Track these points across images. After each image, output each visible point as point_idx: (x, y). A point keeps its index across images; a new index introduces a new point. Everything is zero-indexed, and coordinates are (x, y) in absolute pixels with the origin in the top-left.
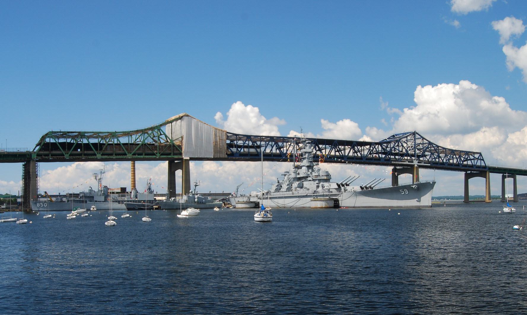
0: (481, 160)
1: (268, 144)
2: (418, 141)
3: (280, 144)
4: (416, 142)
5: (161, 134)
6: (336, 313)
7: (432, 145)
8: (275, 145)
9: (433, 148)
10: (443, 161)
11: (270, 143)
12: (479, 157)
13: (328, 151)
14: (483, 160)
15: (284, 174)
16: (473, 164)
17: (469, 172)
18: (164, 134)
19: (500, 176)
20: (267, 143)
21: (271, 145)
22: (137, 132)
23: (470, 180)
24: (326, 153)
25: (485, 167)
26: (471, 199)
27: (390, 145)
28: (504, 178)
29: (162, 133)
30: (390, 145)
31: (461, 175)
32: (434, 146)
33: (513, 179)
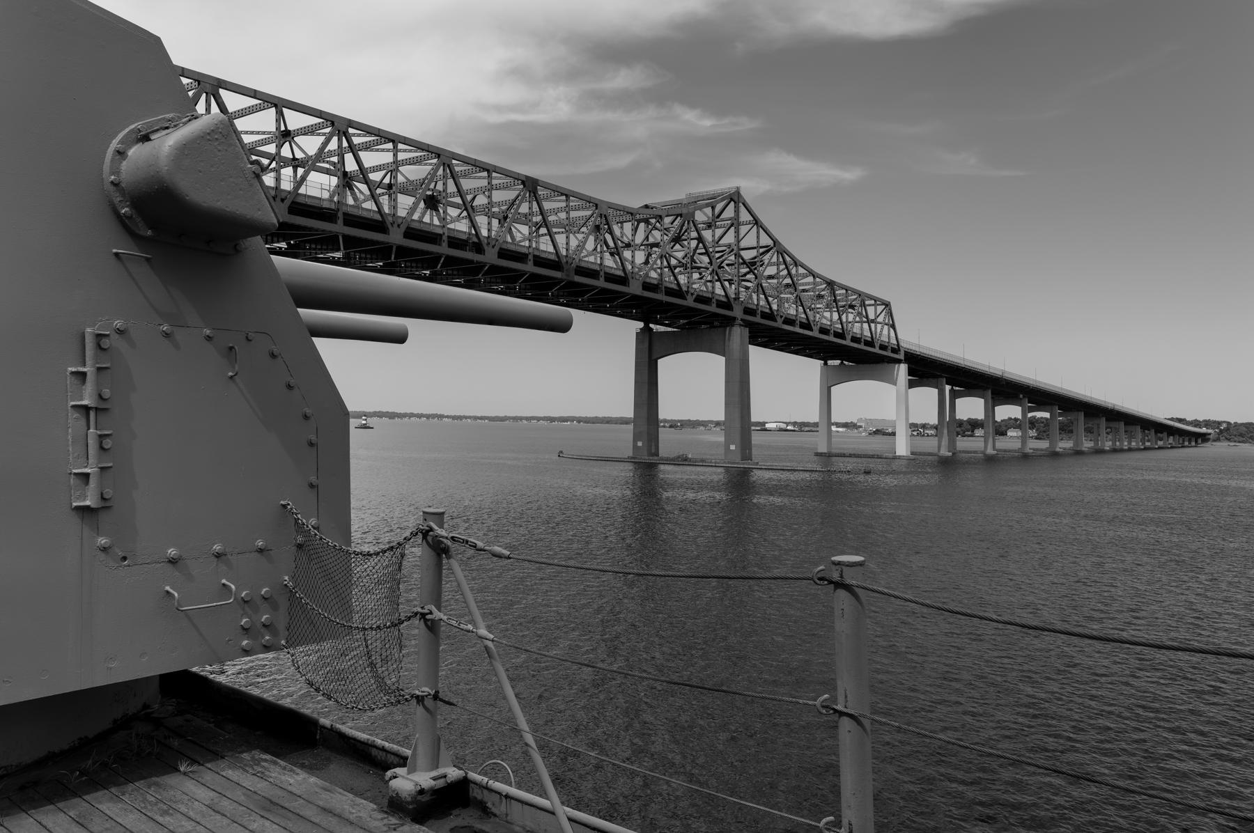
14: (893, 326)
23: (958, 401)
32: (788, 259)
33: (983, 400)
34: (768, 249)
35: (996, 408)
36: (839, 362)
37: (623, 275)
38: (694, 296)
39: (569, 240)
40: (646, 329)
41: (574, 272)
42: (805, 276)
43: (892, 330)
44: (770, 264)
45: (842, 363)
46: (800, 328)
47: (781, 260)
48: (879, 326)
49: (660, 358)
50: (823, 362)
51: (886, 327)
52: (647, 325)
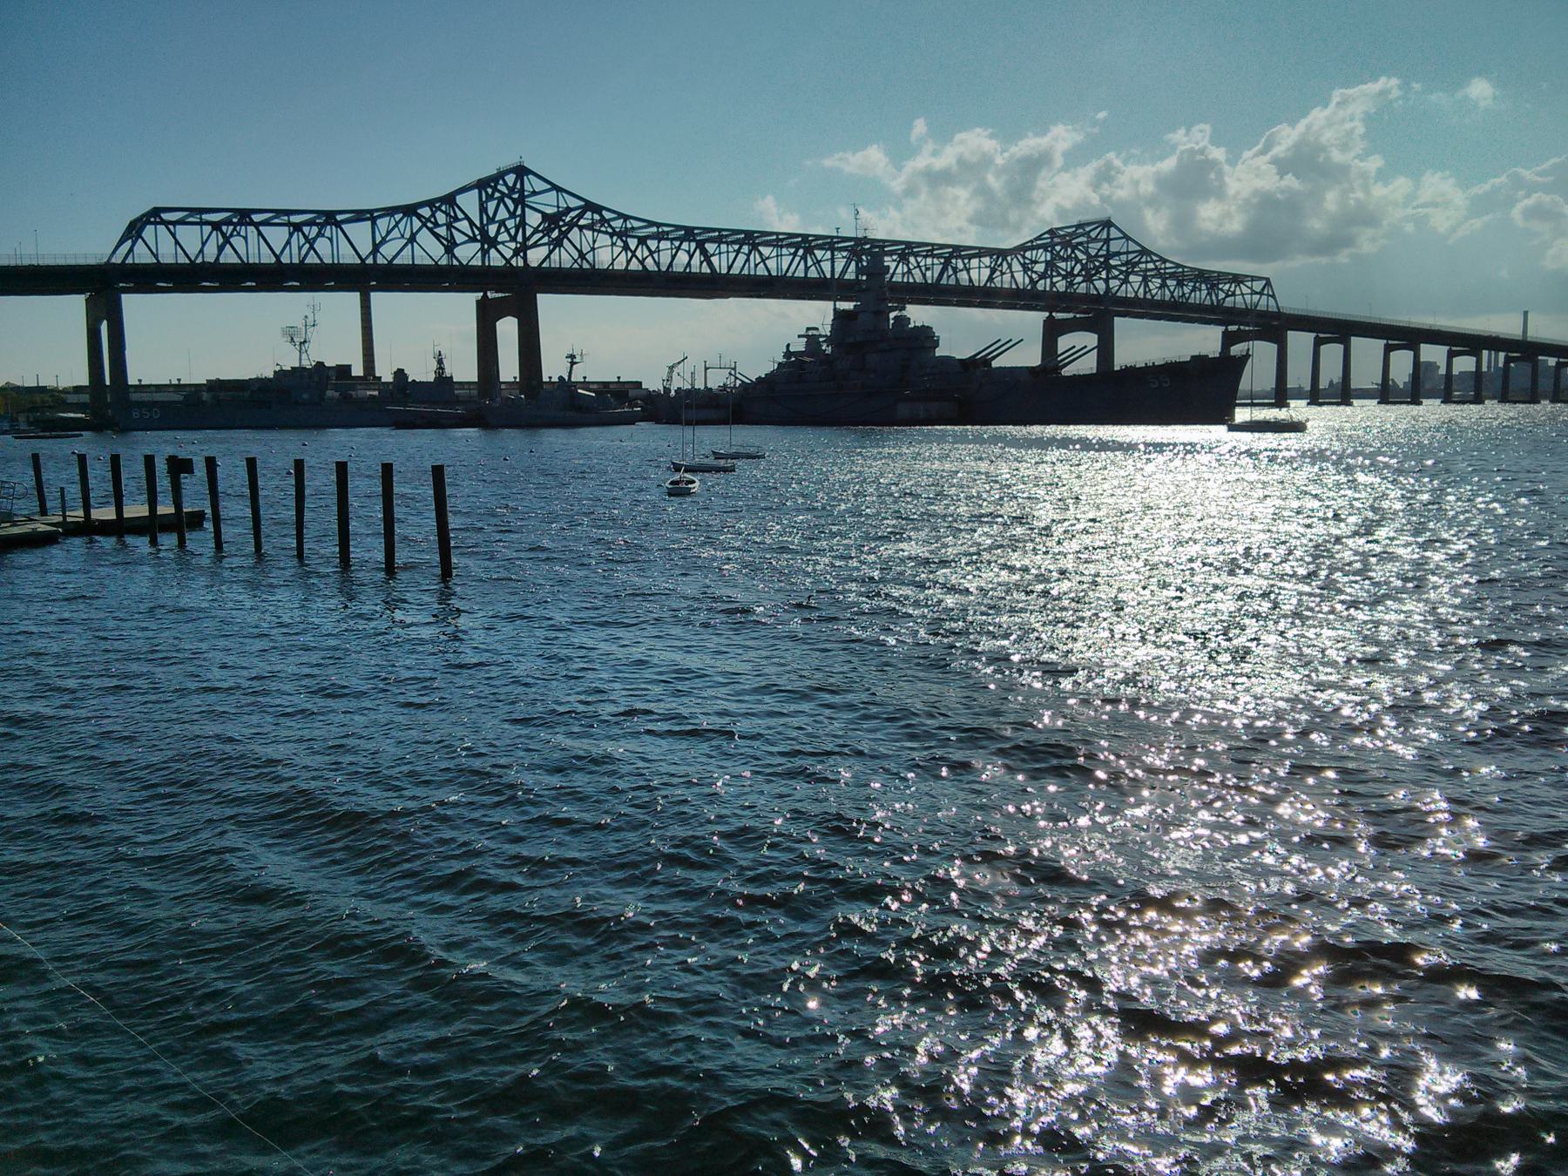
1: (678, 249)
2: (1115, 246)
3: (711, 247)
5: (457, 219)
6: (1555, 1097)
8: (698, 252)
9: (1151, 266)
10: (1172, 296)
11: (685, 245)
12: (1263, 289)
13: (786, 261)
14: (1273, 296)
15: (803, 333)
16: (828, 276)
18: (467, 218)
19: (1380, 344)
20: (677, 243)
21: (688, 252)
22: (390, 211)
28: (1388, 349)
29: (460, 215)
31: (464, 305)
32: (1155, 258)
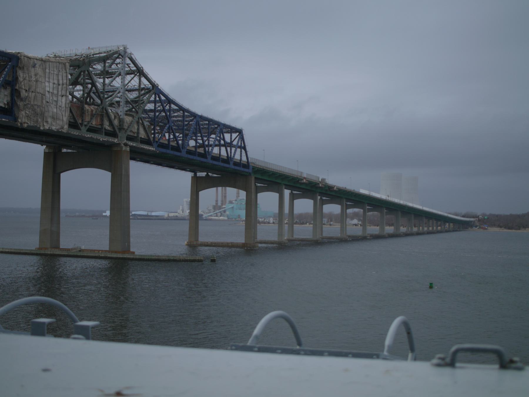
0: (240, 147)
4: (113, 83)
7: (159, 97)
14: (244, 148)
17: (204, 174)
23: (296, 202)
24: (134, 77)
25: (247, 165)
26: (339, 227)
27: (132, 79)
30: (132, 79)
32: (163, 98)
33: (109, 174)
34: (148, 91)
35: (64, 176)
36: (206, 173)
37: (112, 130)
38: (87, 127)
39: (236, 152)
40: (292, 192)
41: (126, 139)
42: (175, 111)
43: (243, 151)
44: (150, 102)
45: (207, 174)
46: (243, 167)
47: (158, 99)
48: (233, 149)
49: (200, 191)
50: (193, 173)
51: (239, 150)
52: (195, 174)
